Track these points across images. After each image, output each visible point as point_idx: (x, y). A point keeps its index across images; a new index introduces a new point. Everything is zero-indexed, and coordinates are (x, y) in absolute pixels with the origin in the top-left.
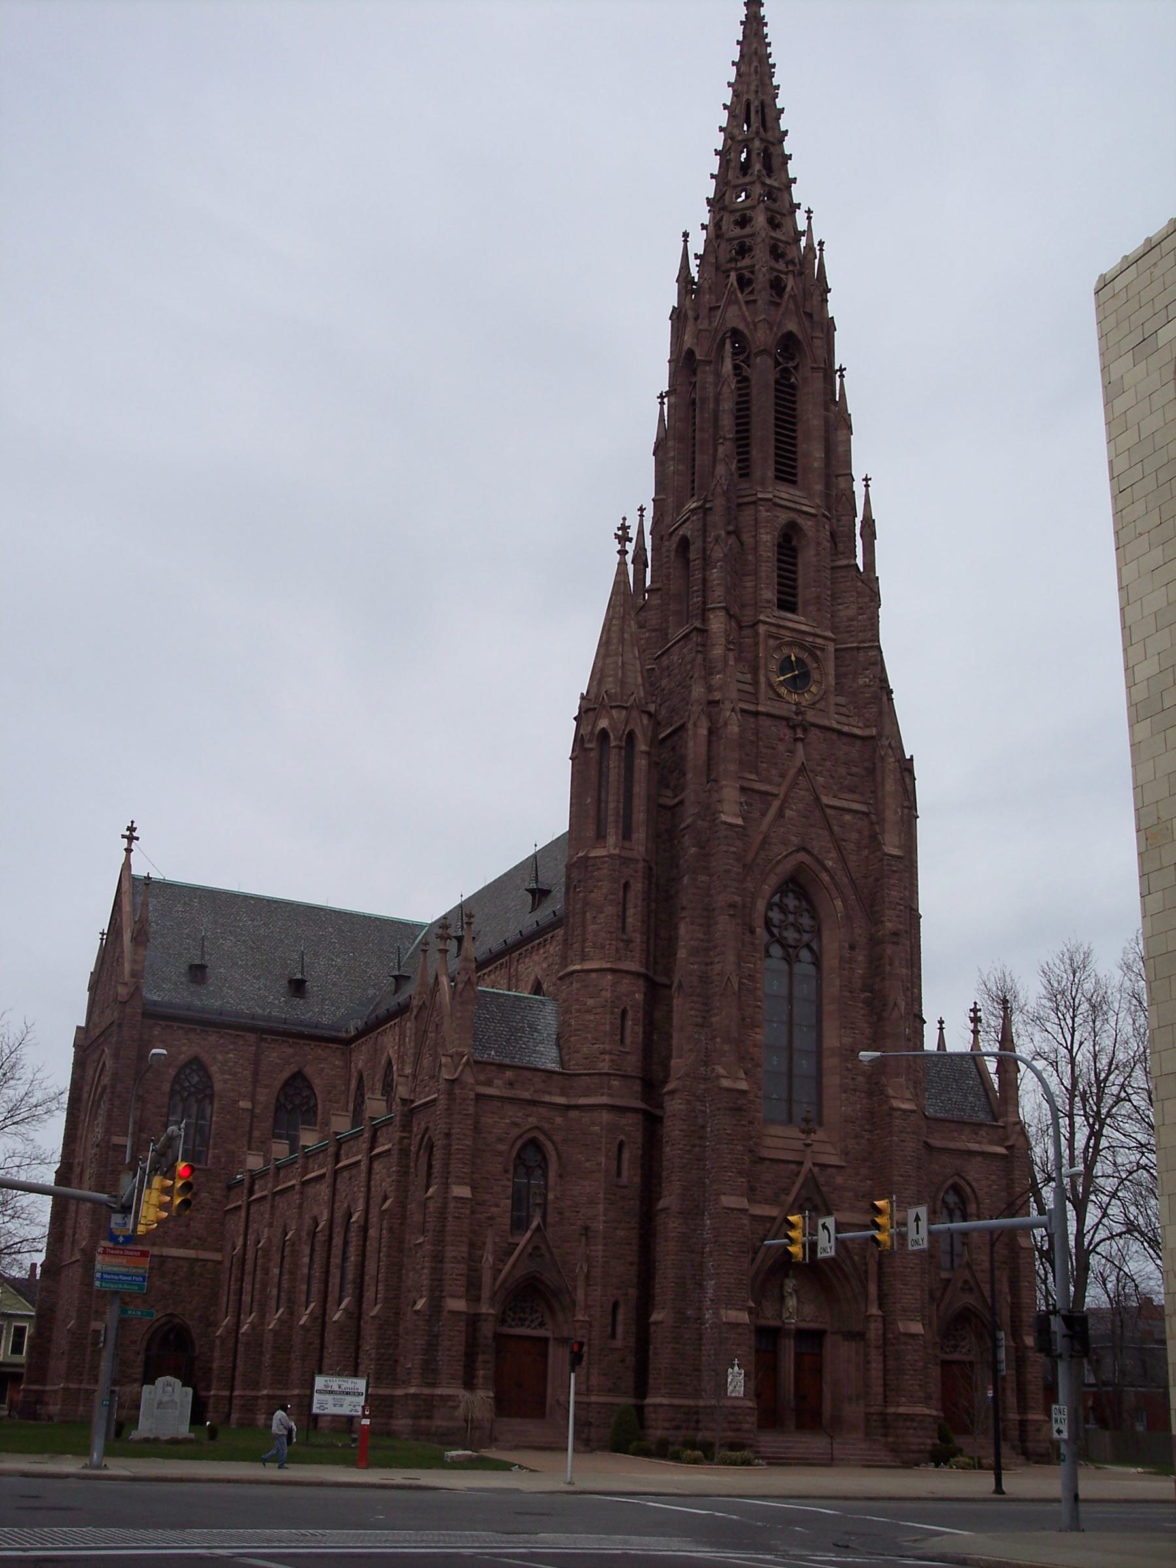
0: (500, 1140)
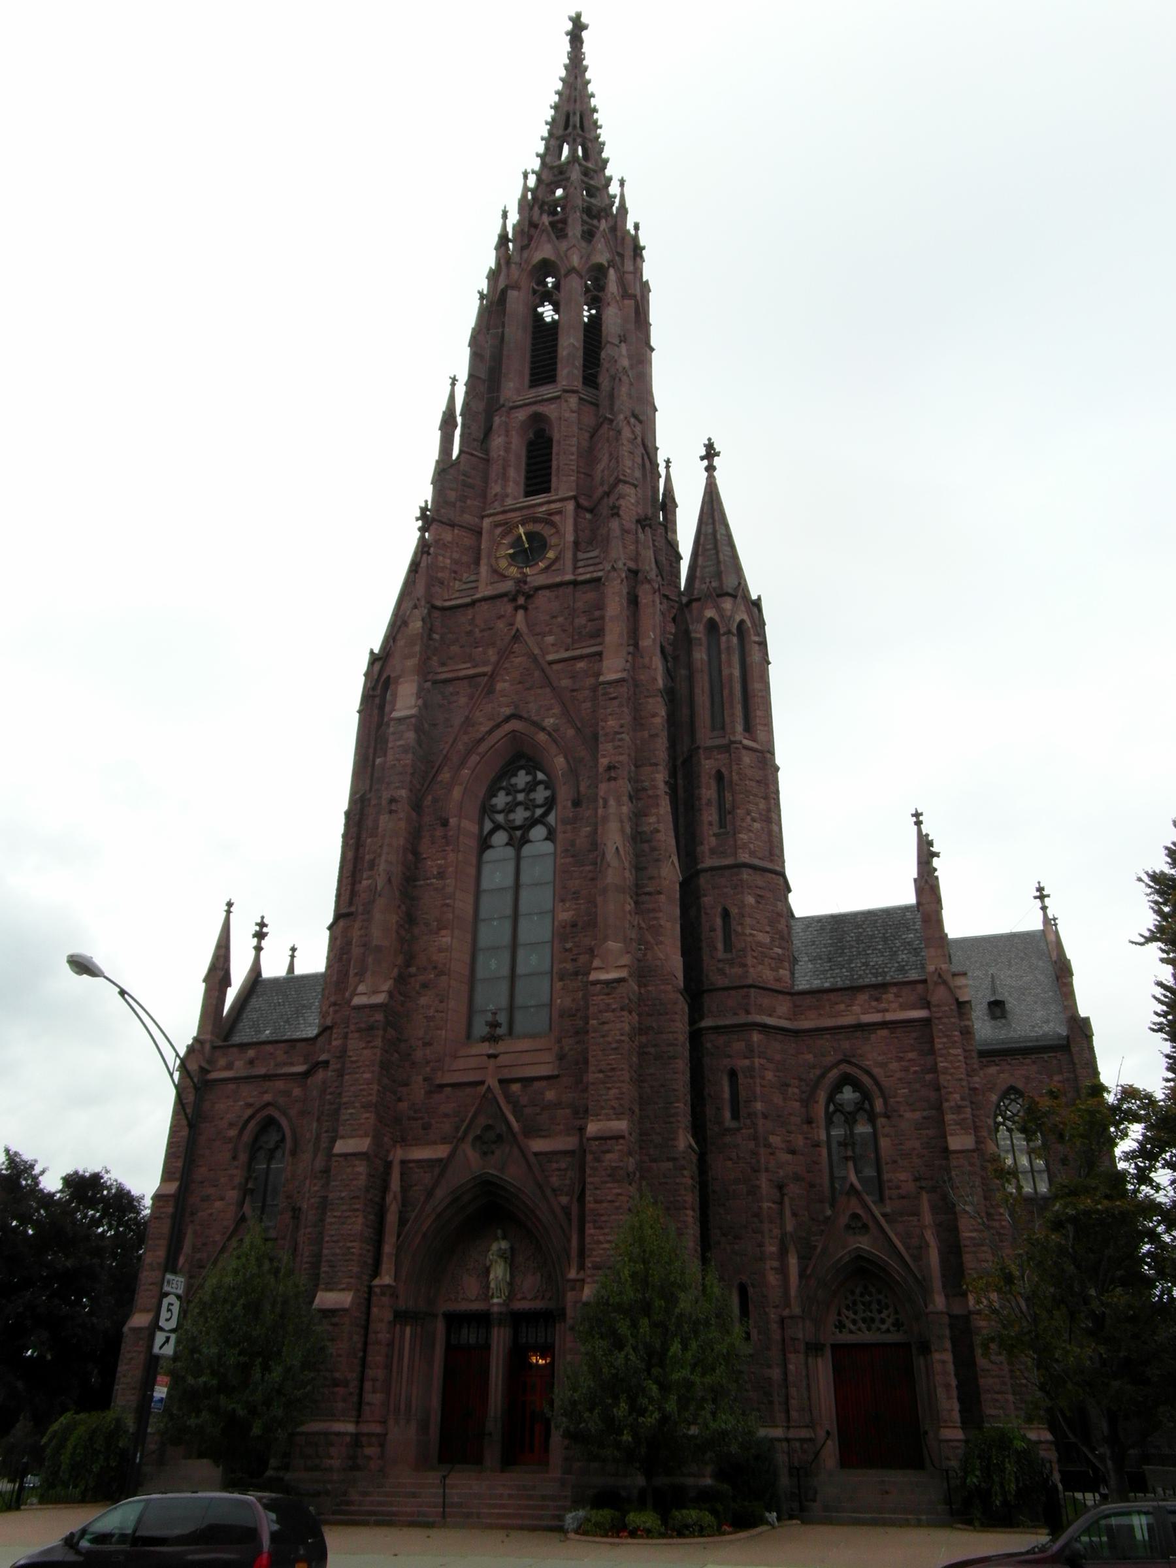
0: (231, 1125)
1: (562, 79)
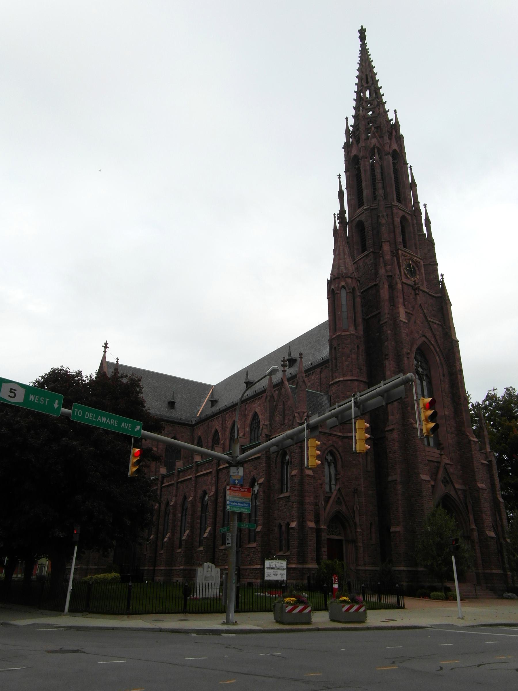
1: (357, 77)
